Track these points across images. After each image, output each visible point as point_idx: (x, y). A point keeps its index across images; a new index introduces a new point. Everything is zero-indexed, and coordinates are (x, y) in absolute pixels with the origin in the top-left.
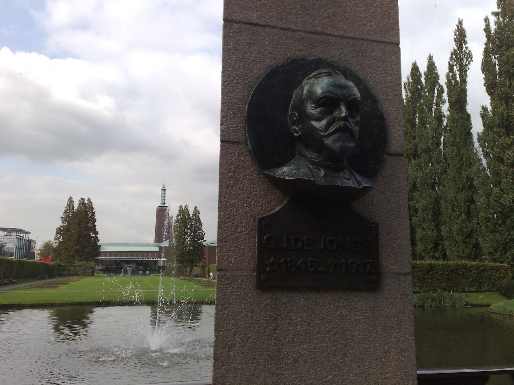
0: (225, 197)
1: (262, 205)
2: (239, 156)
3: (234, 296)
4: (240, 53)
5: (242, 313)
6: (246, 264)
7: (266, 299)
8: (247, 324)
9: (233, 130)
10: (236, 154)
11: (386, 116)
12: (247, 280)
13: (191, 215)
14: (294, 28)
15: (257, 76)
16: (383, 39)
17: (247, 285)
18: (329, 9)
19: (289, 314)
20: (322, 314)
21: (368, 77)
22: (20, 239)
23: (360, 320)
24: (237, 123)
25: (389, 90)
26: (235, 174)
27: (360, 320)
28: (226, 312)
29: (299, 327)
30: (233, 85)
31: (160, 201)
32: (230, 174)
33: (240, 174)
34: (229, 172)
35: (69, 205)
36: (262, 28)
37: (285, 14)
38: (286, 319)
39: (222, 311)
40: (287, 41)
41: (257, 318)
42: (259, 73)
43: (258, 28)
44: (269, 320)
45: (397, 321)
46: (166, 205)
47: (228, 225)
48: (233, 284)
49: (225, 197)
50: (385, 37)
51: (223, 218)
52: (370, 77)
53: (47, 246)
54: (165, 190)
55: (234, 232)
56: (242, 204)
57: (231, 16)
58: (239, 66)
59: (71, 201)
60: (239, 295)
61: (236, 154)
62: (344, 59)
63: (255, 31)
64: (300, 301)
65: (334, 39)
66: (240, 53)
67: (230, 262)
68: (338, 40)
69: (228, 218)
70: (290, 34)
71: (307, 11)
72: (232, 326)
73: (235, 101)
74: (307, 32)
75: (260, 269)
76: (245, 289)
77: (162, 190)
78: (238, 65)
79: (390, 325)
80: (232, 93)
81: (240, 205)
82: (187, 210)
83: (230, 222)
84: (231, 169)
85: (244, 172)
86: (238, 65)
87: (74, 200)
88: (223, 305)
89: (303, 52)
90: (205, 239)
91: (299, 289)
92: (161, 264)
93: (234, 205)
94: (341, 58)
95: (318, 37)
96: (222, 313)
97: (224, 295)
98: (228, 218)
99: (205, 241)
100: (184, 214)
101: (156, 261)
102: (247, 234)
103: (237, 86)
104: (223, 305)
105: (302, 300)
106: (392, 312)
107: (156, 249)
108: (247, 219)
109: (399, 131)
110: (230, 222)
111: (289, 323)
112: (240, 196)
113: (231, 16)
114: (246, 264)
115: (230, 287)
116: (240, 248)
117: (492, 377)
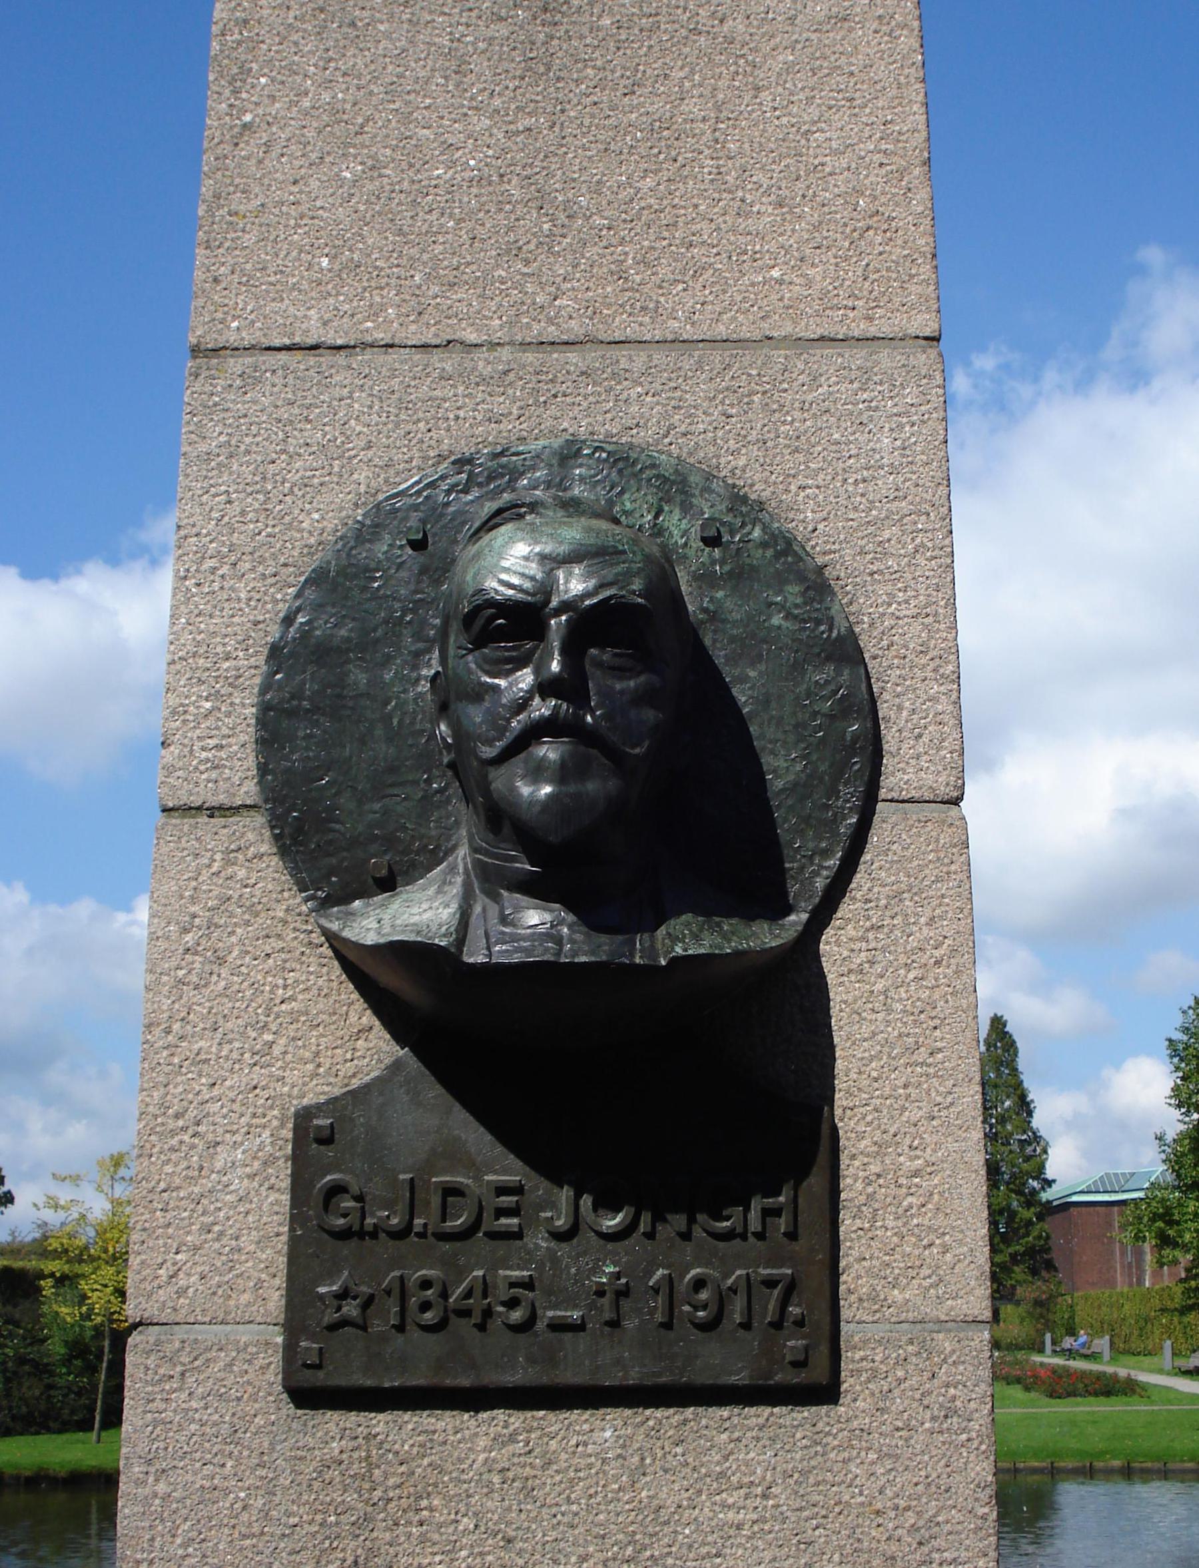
0: (168, 1031)
1: (317, 1054)
2: (228, 862)
3: (193, 1427)
4: (248, 464)
5: (227, 1492)
6: (245, 1298)
8: (245, 1537)
9: (208, 760)
10: (218, 857)
11: (869, 646)
12: (250, 1362)
14: (472, 337)
15: (312, 541)
16: (859, 328)
17: (249, 1383)
18: (622, 242)
19: (424, 1503)
20: (569, 1501)
21: (793, 488)
23: (739, 1527)
24: (225, 731)
25: (886, 534)
26: (209, 936)
27: (739, 1527)
28: (162, 1488)
29: (464, 1553)
30: (216, 586)
32: (189, 938)
33: (233, 933)
34: (186, 931)
36: (341, 358)
37: (436, 289)
38: (409, 1523)
39: (145, 1482)
40: (438, 393)
41: (289, 1515)
42: (323, 530)
43: (326, 359)
44: (337, 1523)
45: (914, 1529)
47: (174, 1142)
48: (190, 1380)
49: (168, 1031)
50: (870, 319)
51: (156, 1117)
52: (802, 488)
55: (201, 1168)
56: (235, 1055)
57: (220, 332)
58: (243, 513)
60: (215, 1424)
61: (218, 857)
62: (683, 429)
63: (312, 372)
65: (643, 356)
66: (248, 464)
67: (182, 1292)
68: (659, 357)
69: (177, 1116)
70: (447, 362)
71: (527, 262)
72: (185, 1545)
73: (219, 649)
74: (525, 345)
76: (239, 1399)
78: (237, 507)
79: (883, 1546)
80: (211, 616)
81: (227, 1058)
83: (184, 1129)
84: (194, 916)
85: (247, 923)
86: (237, 507)
88: (149, 1462)
89: (505, 426)
93: (199, 1060)
94: (672, 427)
95: (573, 357)
96: (147, 1491)
97: (156, 1423)
98: (177, 1116)
102: (251, 1177)
103: (232, 589)
104: (149, 1462)
105: (482, 1442)
106: (889, 1492)
108: (254, 1115)
109: (934, 699)
110: (184, 1129)
111: (423, 1540)
112: (229, 1025)
113: (220, 332)
114: (245, 1298)
115: (180, 1389)
116: (221, 1234)
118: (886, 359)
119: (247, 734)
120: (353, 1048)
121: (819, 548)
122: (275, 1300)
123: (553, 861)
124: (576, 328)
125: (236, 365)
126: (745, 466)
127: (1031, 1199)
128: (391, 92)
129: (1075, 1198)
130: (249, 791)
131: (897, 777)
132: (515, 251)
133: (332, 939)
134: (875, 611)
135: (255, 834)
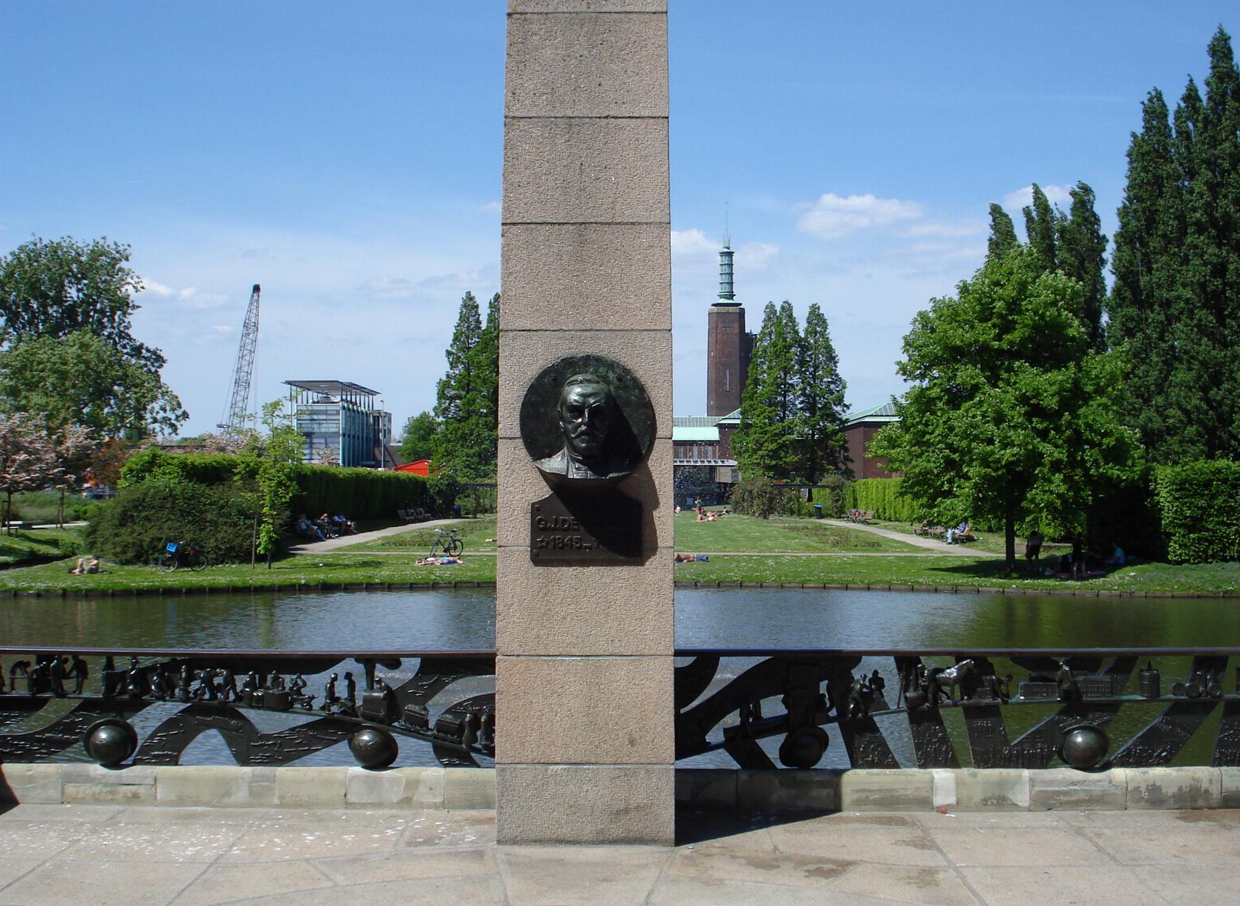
7: (540, 569)
13: (802, 335)
22: (352, 413)
31: (718, 290)
35: (463, 318)
46: (736, 300)
53: (422, 428)
54: (730, 254)
59: (470, 305)
64: (568, 574)
70: (561, 334)
75: (533, 545)
77: (722, 254)
82: (790, 316)
87: (478, 301)
90: (846, 402)
91: (569, 563)
92: (724, 477)
99: (848, 407)
100: (780, 335)
101: (712, 469)
107: (713, 434)
117: (864, 658)
118: (659, 335)
119: (518, 422)
120: (545, 492)
121: (643, 381)
122: (528, 542)
123: (587, 459)
124: (588, 327)
125: (511, 334)
126: (630, 365)
127: (833, 417)
128: (544, 265)
129: (867, 420)
130: (518, 434)
131: (660, 433)
132: (574, 306)
133: (543, 473)
134: (656, 396)
135: (520, 443)
